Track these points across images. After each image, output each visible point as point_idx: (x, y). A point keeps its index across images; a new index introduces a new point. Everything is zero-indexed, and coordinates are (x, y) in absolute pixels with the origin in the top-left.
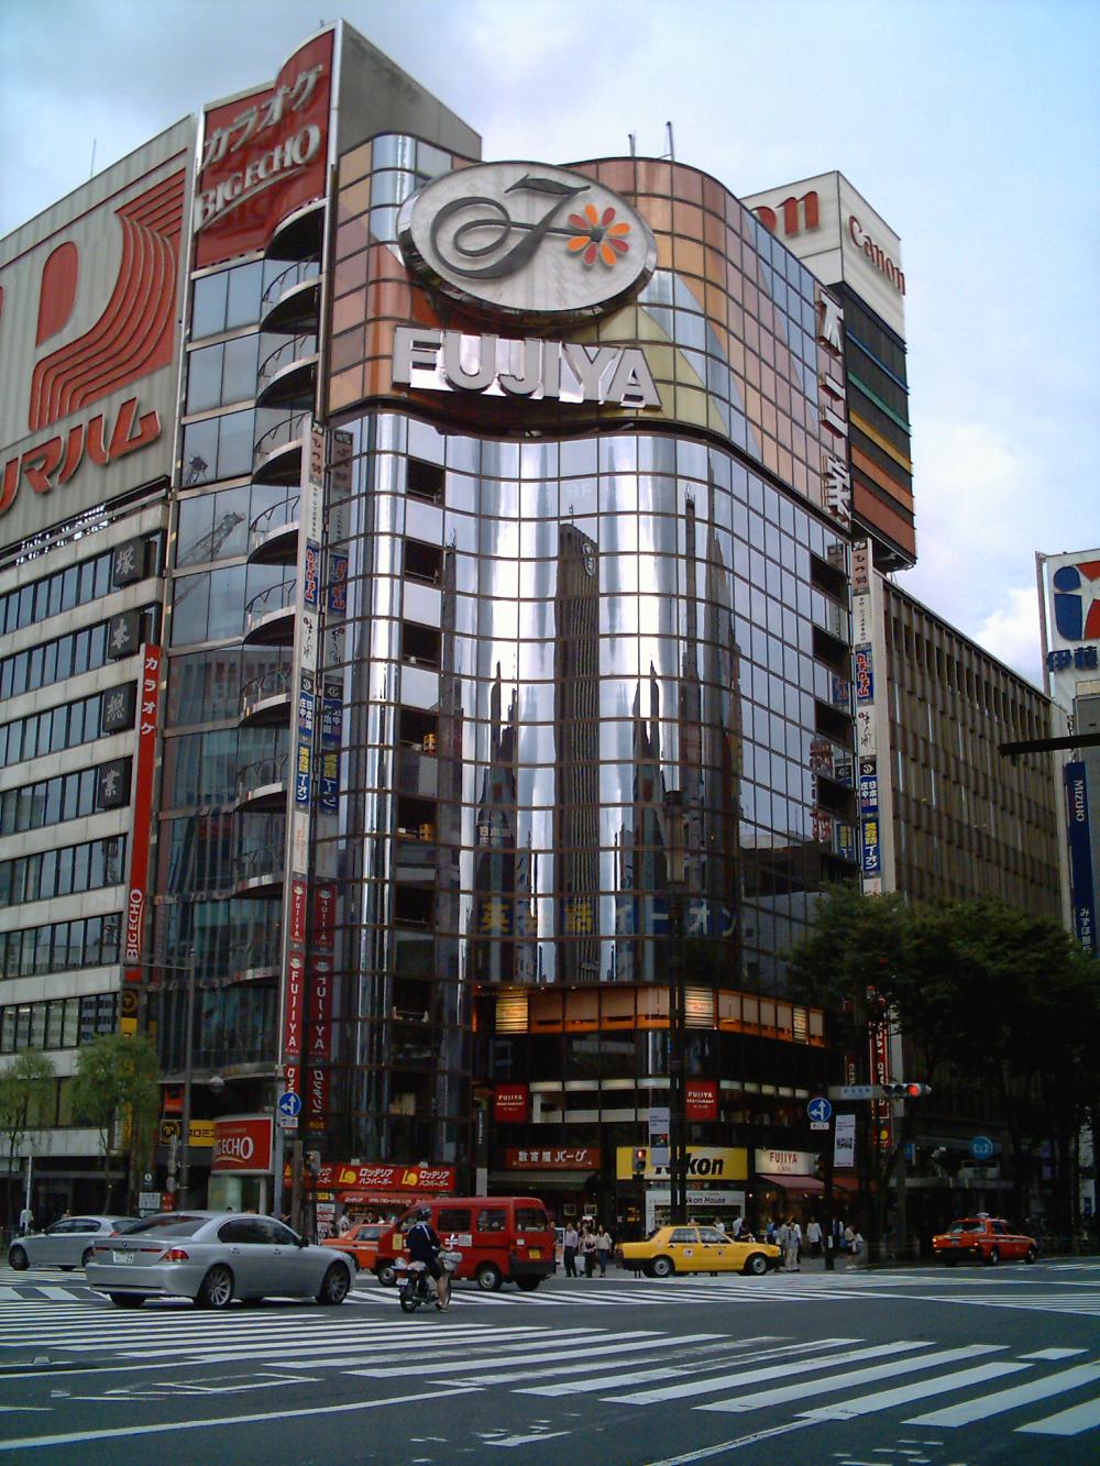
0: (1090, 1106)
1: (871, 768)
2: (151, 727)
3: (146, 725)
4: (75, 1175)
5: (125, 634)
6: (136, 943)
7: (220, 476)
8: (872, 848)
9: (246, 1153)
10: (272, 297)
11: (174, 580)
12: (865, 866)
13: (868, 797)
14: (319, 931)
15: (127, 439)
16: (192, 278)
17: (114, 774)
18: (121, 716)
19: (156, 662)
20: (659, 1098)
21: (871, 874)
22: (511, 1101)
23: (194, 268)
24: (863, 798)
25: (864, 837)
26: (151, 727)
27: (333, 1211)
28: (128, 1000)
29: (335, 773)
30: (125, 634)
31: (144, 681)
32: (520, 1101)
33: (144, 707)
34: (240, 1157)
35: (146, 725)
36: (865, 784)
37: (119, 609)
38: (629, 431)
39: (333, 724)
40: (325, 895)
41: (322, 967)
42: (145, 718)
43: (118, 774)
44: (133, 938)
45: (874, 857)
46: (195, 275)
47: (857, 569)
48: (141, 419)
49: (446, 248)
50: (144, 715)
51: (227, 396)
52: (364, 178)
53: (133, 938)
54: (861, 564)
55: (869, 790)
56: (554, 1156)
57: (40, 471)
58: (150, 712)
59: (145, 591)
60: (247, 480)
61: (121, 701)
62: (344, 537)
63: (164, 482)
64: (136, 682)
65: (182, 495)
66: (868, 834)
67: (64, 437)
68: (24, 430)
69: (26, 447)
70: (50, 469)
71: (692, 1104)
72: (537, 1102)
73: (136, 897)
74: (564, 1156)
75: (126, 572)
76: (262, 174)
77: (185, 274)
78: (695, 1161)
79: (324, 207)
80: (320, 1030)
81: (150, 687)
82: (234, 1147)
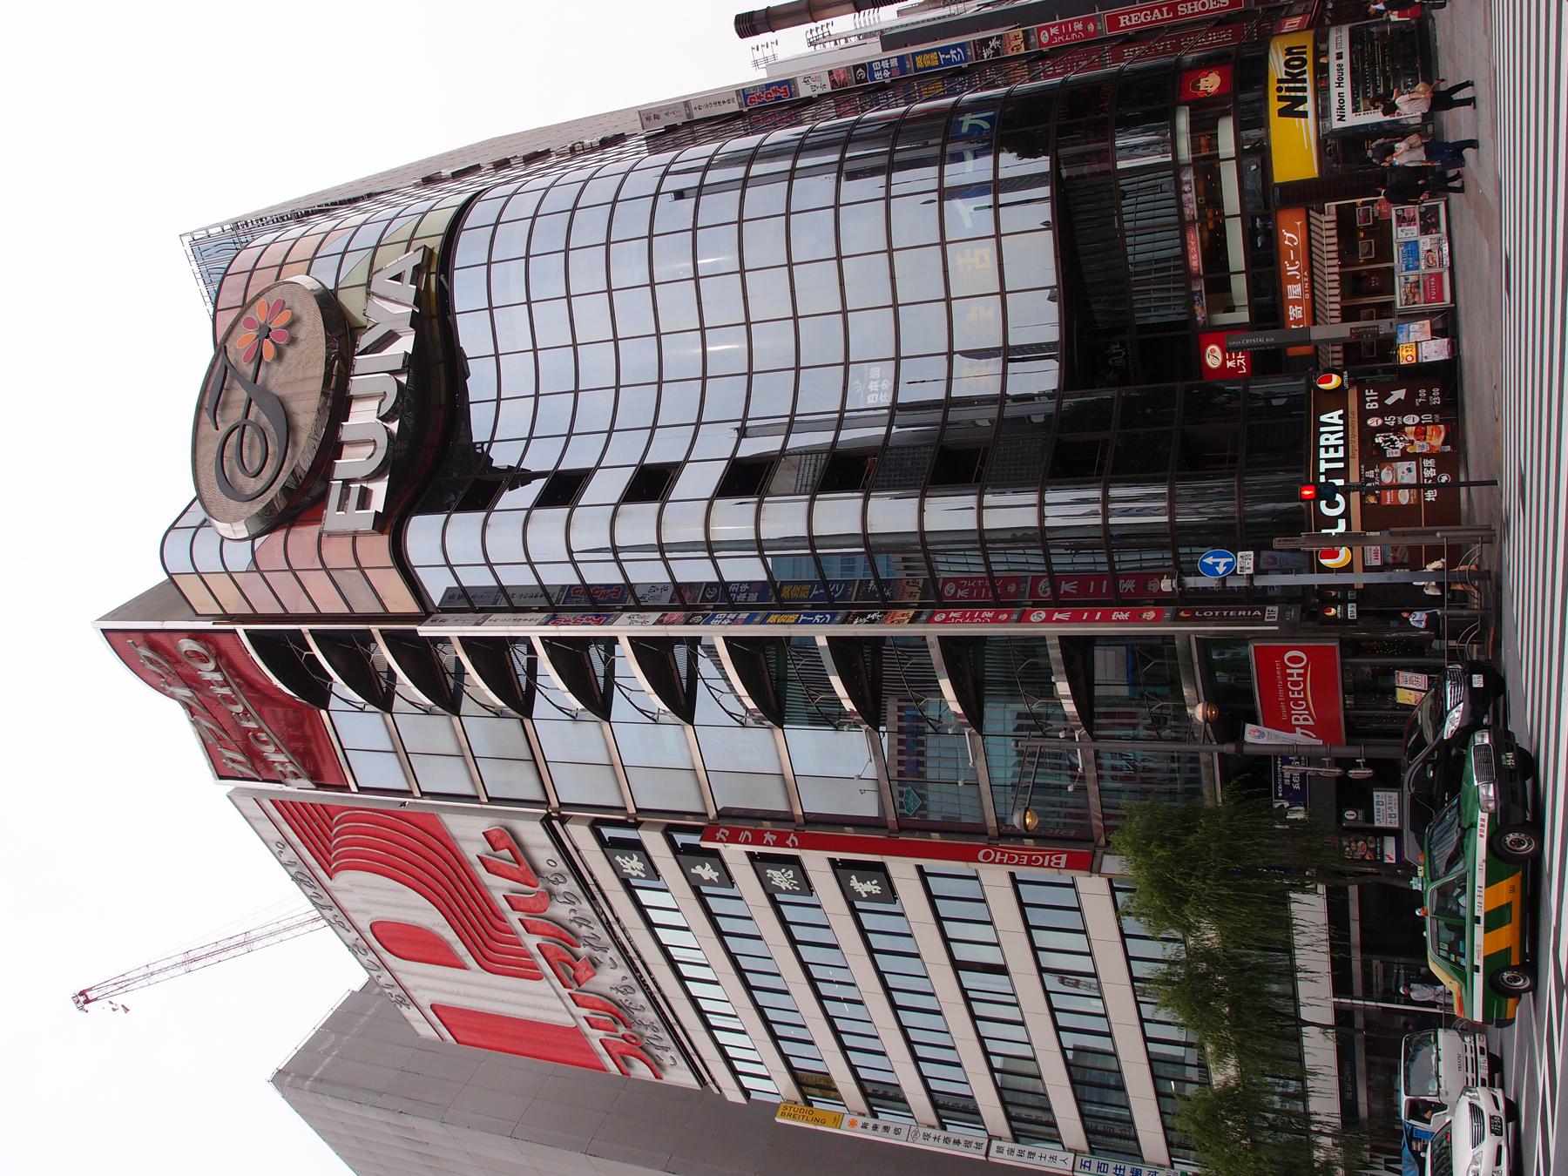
1: (860, 70)
2: (792, 837)
3: (789, 842)
4: (1356, 956)
6: (1044, 856)
7: (527, 755)
8: (942, 57)
9: (1301, 660)
10: (361, 706)
12: (961, 61)
15: (517, 866)
16: (356, 791)
17: (854, 883)
18: (790, 872)
19: (722, 830)
23: (346, 788)
24: (890, 76)
25: (930, 68)
26: (792, 837)
29: (804, 587)
31: (740, 843)
33: (768, 844)
34: (1305, 668)
35: (789, 842)
38: (449, 278)
39: (748, 591)
42: (780, 842)
43: (853, 877)
44: (1037, 860)
45: (952, 52)
46: (354, 788)
48: (495, 850)
49: (253, 485)
50: (776, 844)
51: (454, 750)
52: (203, 580)
53: (1037, 860)
55: (882, 69)
56: (1293, 280)
57: (574, 968)
58: (775, 837)
59: (654, 841)
60: (527, 722)
61: (775, 873)
62: (541, 592)
63: (547, 821)
65: (554, 803)
66: (928, 64)
67: (538, 939)
68: (542, 986)
69: (557, 983)
70: (569, 957)
73: (987, 856)
76: (240, 709)
77: (352, 798)
78: (1287, 73)
79: (245, 630)
82: (1295, 678)
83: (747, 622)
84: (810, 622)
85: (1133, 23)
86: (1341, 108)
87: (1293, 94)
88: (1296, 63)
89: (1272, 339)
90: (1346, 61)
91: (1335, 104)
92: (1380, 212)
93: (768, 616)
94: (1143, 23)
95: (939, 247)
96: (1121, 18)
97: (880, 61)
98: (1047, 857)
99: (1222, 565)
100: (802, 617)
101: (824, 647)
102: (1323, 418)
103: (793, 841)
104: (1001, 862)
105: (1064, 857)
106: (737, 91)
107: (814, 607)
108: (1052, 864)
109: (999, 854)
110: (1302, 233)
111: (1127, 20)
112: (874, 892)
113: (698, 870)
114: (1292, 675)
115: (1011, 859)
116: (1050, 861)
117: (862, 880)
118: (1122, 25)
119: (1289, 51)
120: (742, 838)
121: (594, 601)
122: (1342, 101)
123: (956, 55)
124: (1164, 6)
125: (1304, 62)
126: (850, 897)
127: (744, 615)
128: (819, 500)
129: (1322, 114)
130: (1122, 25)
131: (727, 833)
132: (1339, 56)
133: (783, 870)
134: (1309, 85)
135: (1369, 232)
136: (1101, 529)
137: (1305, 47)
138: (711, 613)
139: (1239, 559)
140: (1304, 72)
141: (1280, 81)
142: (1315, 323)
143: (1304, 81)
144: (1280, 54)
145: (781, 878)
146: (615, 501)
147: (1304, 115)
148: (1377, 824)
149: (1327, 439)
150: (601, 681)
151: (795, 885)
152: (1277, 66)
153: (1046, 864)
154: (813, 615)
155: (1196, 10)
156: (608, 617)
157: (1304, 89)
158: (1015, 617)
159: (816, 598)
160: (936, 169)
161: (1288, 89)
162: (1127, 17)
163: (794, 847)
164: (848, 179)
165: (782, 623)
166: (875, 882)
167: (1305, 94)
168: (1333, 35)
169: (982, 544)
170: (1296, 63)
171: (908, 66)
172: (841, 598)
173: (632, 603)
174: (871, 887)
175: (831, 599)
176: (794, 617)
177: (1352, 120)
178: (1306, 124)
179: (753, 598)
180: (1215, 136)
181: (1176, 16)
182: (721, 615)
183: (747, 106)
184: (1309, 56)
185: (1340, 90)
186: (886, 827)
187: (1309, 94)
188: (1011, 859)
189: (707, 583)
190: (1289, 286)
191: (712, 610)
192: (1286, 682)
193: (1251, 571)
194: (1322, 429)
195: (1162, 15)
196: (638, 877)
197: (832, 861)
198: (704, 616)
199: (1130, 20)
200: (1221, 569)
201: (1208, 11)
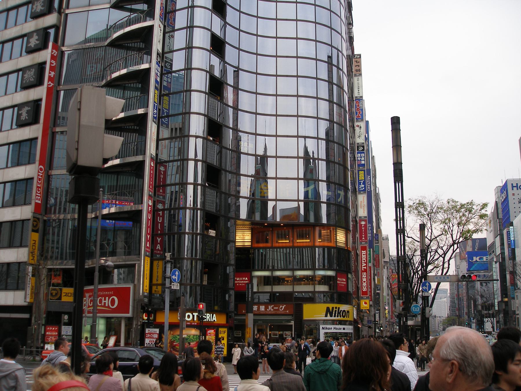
0: (278, 296)
1: (362, 148)
2: (52, 84)
5: (36, 40)
8: (362, 181)
11: (67, 15)
12: (359, 189)
13: (360, 160)
14: (159, 186)
18: (33, 80)
19: (56, 52)
20: (325, 280)
21: (361, 192)
22: (241, 280)
24: (358, 160)
26: (52, 84)
27: (158, 332)
28: (35, 223)
29: (168, 106)
30: (36, 40)
31: (51, 60)
32: (246, 280)
33: (50, 73)
34: (108, 307)
35: (50, 83)
36: (359, 155)
37: (33, 29)
39: (168, 81)
40: (162, 169)
41: (160, 206)
42: (50, 79)
43: (30, 108)
47: (356, 66)
50: (49, 77)
53: (39, 191)
54: (357, 64)
58: (52, 76)
59: (51, 19)
64: (45, 63)
71: (339, 284)
72: (255, 281)
73: (41, 169)
74: (272, 308)
75: (39, 11)
78: (341, 311)
80: (159, 240)
81: (53, 64)
82: (103, 301)
83: (156, 81)
84: (154, 108)
85: (362, 256)
86: (327, 329)
87: (334, 312)
88: (344, 314)
89: (250, 300)
90: (342, 331)
91: (328, 326)
92: (288, 340)
93: (158, 90)
94: (362, 259)
95: (297, 177)
96: (365, 251)
97: (364, 157)
98: (40, 195)
99: (175, 277)
100: (156, 105)
101: (137, 111)
102: (214, 315)
103: (50, 84)
104: (39, 175)
105: (40, 202)
106: (362, 97)
107: (159, 110)
108: (37, 197)
109: (42, 174)
110: (283, 313)
111: (364, 253)
112: (22, 117)
113: (35, 37)
114: (105, 300)
115: (40, 179)
116: (38, 196)
117: (28, 112)
118: (362, 252)
119: (348, 312)
120: (53, 62)
121: (169, 13)
122: (329, 329)
123: (362, 187)
124: (367, 268)
125: (344, 317)
126: (20, 106)
127: (158, 79)
128: (205, 118)
129: (325, 322)
130: (362, 252)
131: (55, 55)
132: (344, 329)
133: (34, 77)
134: (336, 318)
135: (281, 336)
136: (184, 231)
137: (349, 317)
138: (160, 65)
139: (177, 284)
140: (340, 317)
141: (339, 308)
142: (254, 315)
143: (338, 317)
144: (348, 309)
145: (31, 76)
146: (212, 30)
147: (326, 316)
148: (63, 327)
149: (208, 316)
150: (129, 7)
151: (26, 81)
152: (344, 307)
153: (37, 194)
154: (156, 110)
155: (363, 279)
156: (162, 19)
157: (338, 317)
158: (151, 193)
159: (163, 110)
160: (325, 179)
161: (336, 311)
162: (365, 254)
163: (48, 85)
164: (234, 71)
165: (155, 96)
166: (27, 118)
167: (333, 317)
168: (351, 327)
169: (181, 183)
170: (344, 314)
171: (360, 167)
172: (162, 122)
173: (167, 30)
174: (24, 116)
175: (162, 117)
176: (156, 101)
177: (322, 332)
178: (323, 316)
179: (165, 84)
180: (322, 284)
181: (362, 271)
182: (159, 69)
183: (356, 100)
184: (345, 319)
185: (333, 328)
186: (54, 126)
187: (333, 318)
188: (40, 179)
189: (172, 64)
190: (264, 306)
191: (161, 65)
192: (102, 296)
193: (172, 288)
194: (211, 315)
195: (363, 267)
196: (32, 8)
197: (41, 100)
198: (159, 62)
199: (364, 255)
200: (174, 277)
201: (362, 283)
